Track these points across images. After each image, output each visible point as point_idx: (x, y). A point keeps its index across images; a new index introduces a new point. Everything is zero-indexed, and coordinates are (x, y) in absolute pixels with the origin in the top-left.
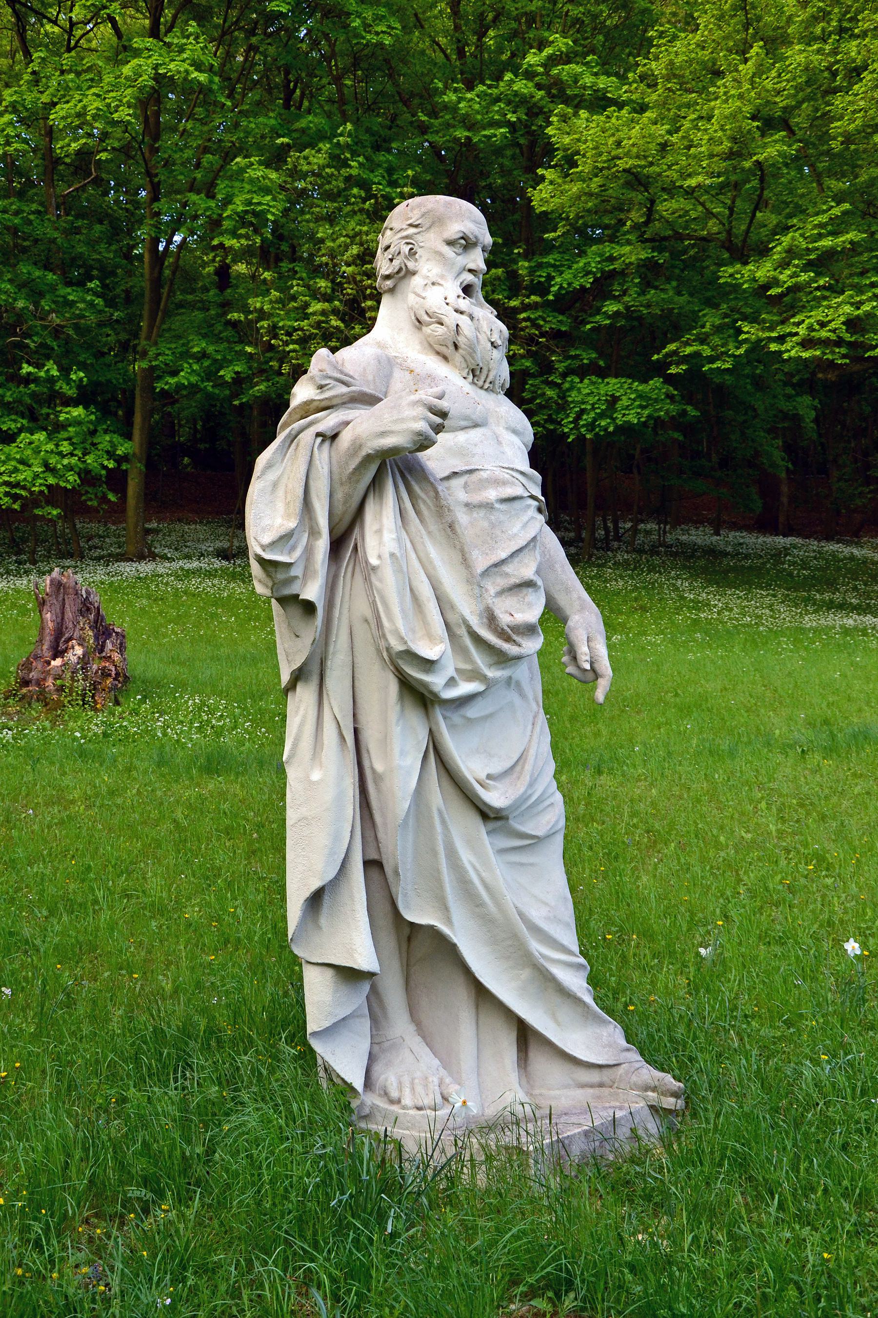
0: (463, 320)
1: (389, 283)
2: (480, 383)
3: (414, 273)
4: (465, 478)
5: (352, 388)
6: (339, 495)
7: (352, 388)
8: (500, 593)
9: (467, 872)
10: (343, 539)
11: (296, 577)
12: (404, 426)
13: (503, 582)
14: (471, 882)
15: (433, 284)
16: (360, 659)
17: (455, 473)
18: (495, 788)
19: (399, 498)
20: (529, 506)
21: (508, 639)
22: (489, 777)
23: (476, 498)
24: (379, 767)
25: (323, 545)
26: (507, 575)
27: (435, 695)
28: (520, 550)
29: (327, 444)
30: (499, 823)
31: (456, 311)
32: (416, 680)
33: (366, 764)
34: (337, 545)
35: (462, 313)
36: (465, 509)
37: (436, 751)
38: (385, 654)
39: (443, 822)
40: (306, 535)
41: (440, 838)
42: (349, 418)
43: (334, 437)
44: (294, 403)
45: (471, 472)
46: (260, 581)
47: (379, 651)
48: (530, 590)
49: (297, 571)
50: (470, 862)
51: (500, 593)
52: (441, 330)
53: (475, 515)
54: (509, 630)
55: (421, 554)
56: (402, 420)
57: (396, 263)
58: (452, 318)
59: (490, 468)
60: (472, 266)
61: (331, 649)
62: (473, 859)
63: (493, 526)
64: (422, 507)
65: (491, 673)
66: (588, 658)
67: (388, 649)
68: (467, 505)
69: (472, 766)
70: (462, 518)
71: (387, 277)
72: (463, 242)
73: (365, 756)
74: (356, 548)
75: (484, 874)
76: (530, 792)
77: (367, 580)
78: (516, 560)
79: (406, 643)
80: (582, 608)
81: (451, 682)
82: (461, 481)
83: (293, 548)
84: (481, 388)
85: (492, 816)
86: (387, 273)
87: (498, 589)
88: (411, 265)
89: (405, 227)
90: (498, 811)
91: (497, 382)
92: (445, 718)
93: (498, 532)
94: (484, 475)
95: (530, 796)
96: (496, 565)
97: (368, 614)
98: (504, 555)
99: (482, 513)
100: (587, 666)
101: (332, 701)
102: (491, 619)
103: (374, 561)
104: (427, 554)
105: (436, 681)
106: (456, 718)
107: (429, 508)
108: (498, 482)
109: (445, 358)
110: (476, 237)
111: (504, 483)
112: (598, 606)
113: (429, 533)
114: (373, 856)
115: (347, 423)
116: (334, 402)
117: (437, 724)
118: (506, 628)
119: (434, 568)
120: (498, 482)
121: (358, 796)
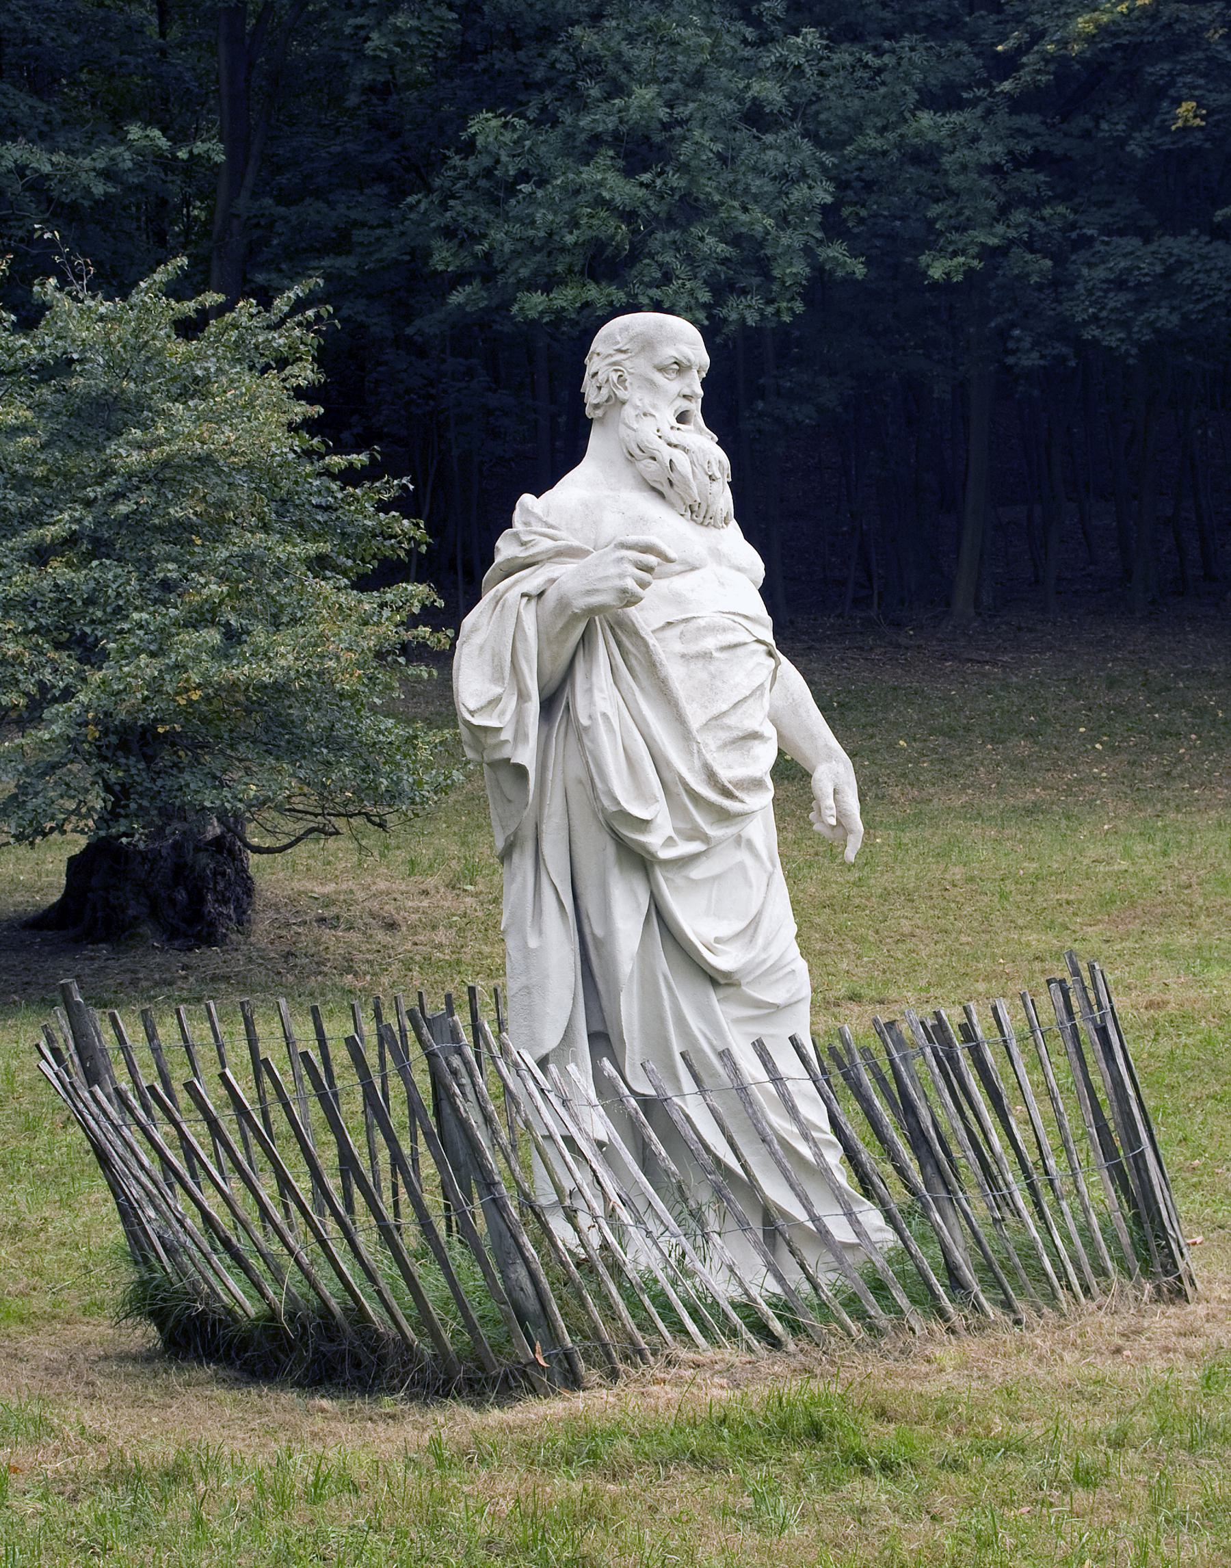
0: (678, 455)
1: (599, 413)
2: (700, 519)
3: (623, 403)
4: (682, 627)
5: (559, 543)
6: (547, 655)
7: (559, 543)
8: (724, 746)
9: (696, 1040)
10: (554, 701)
11: (506, 741)
12: (610, 584)
13: (725, 736)
14: (702, 1051)
15: (645, 415)
16: (576, 822)
17: (669, 624)
18: (725, 952)
19: (610, 655)
20: (754, 652)
21: (727, 793)
22: (717, 940)
23: (693, 648)
24: (599, 932)
25: (534, 706)
26: (729, 728)
27: (653, 855)
28: (745, 699)
29: (533, 602)
30: (731, 990)
31: (670, 444)
32: (632, 840)
33: (587, 930)
34: (548, 705)
35: (676, 446)
36: (681, 661)
37: (658, 914)
38: (600, 816)
39: (669, 988)
40: (515, 698)
41: (667, 1004)
42: (555, 575)
43: (541, 595)
44: (498, 559)
45: (686, 620)
46: (470, 746)
47: (595, 814)
48: (756, 742)
49: (506, 735)
50: (700, 1029)
51: (724, 746)
52: (653, 465)
53: (692, 666)
54: (731, 787)
55: (634, 713)
56: (607, 578)
57: (605, 392)
58: (666, 453)
59: (707, 614)
60: (687, 391)
61: (546, 811)
62: (704, 1028)
63: (713, 677)
64: (634, 662)
65: (713, 832)
66: (834, 812)
67: (603, 809)
68: (683, 656)
69: (696, 923)
70: (675, 672)
71: (596, 406)
72: (676, 367)
73: (585, 921)
74: (567, 707)
75: (715, 1042)
76: (764, 956)
77: (580, 739)
78: (740, 711)
79: (619, 803)
80: (830, 757)
81: (669, 842)
82: (676, 631)
83: (503, 713)
84: (702, 524)
85: (722, 981)
86: (595, 402)
87: (720, 743)
88: (621, 394)
89: (612, 352)
90: (727, 975)
91: (719, 517)
92: (666, 880)
93: (718, 683)
94: (702, 622)
95: (764, 961)
96: (716, 718)
97: (583, 775)
98: (725, 707)
99: (700, 664)
100: (833, 822)
101: (550, 870)
102: (711, 777)
103: (584, 721)
104: (640, 711)
105: (654, 840)
106: (679, 880)
107: (640, 663)
108: (713, 629)
109: (661, 495)
110: (689, 361)
111: (725, 630)
112: (852, 755)
113: (642, 689)
114: (598, 1027)
115: (553, 581)
116: (539, 558)
117: (658, 885)
118: (726, 784)
119: (648, 726)
120: (713, 629)
121: (579, 964)
